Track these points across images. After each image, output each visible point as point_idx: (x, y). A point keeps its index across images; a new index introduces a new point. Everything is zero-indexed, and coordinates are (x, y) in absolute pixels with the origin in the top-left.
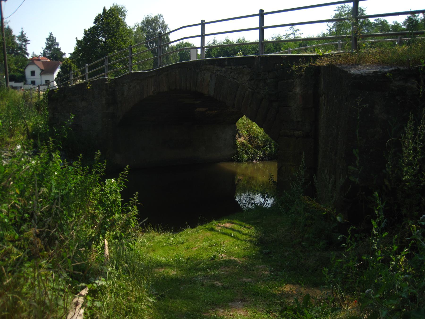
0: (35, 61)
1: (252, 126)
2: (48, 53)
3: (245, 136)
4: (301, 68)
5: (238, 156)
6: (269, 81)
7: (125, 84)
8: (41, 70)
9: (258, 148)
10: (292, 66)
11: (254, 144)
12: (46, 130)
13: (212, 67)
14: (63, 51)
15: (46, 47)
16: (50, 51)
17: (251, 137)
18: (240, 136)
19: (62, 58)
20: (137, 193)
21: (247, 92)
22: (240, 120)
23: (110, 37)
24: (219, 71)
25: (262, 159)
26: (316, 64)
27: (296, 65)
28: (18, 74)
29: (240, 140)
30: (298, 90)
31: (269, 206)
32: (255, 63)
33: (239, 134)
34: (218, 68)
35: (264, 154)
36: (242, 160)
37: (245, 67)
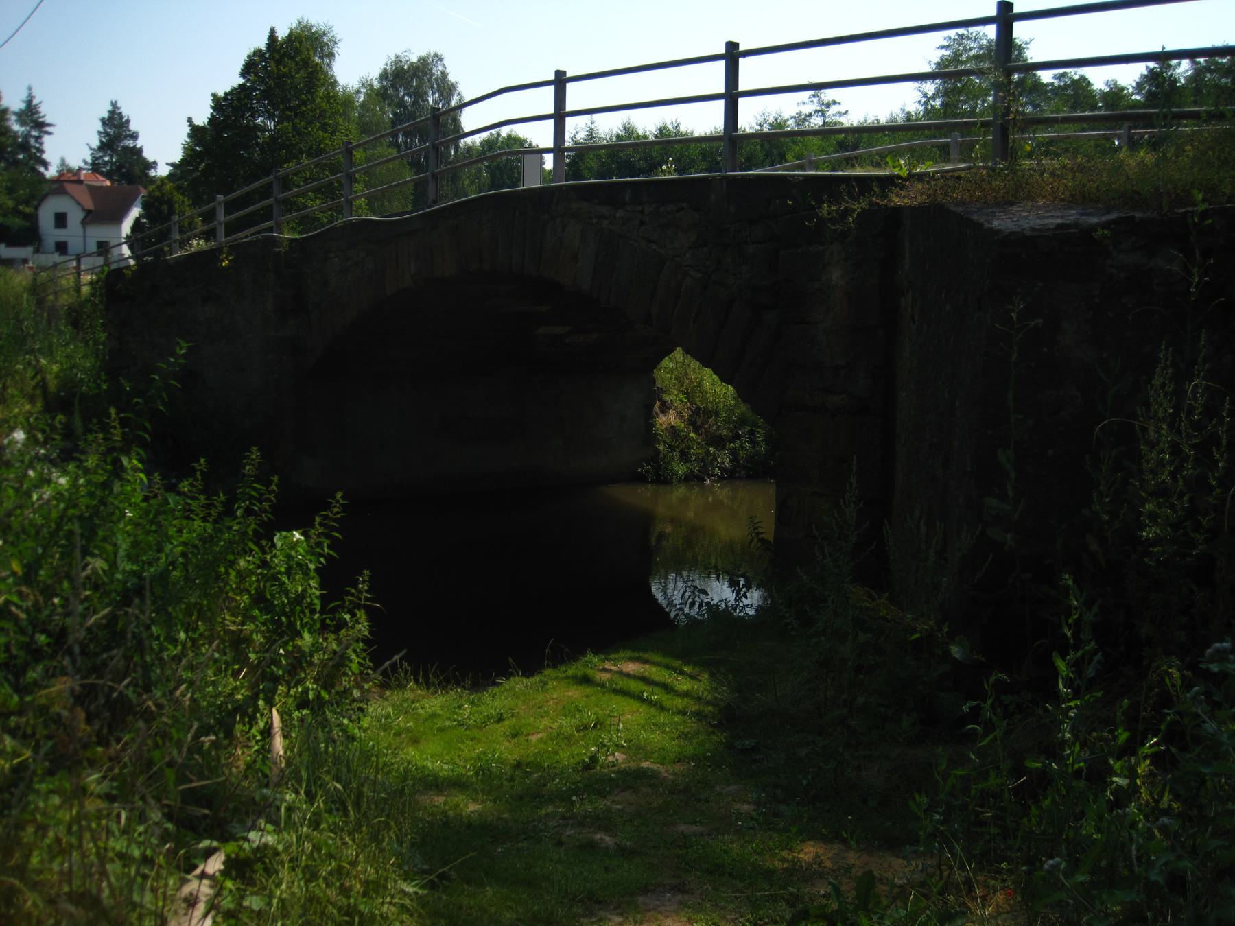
1: (702, 380)
2: (106, 163)
3: (680, 407)
4: (846, 213)
8: (84, 210)
9: (719, 442)
10: (820, 207)
11: (706, 432)
12: (99, 386)
14: (149, 155)
16: (111, 157)
17: (696, 412)
18: (665, 408)
19: (146, 175)
20: (366, 572)
22: (666, 362)
23: (288, 118)
25: (729, 476)
26: (890, 201)
27: (830, 204)
29: (666, 420)
30: (836, 275)
31: (751, 612)
33: (663, 403)
36: (672, 477)
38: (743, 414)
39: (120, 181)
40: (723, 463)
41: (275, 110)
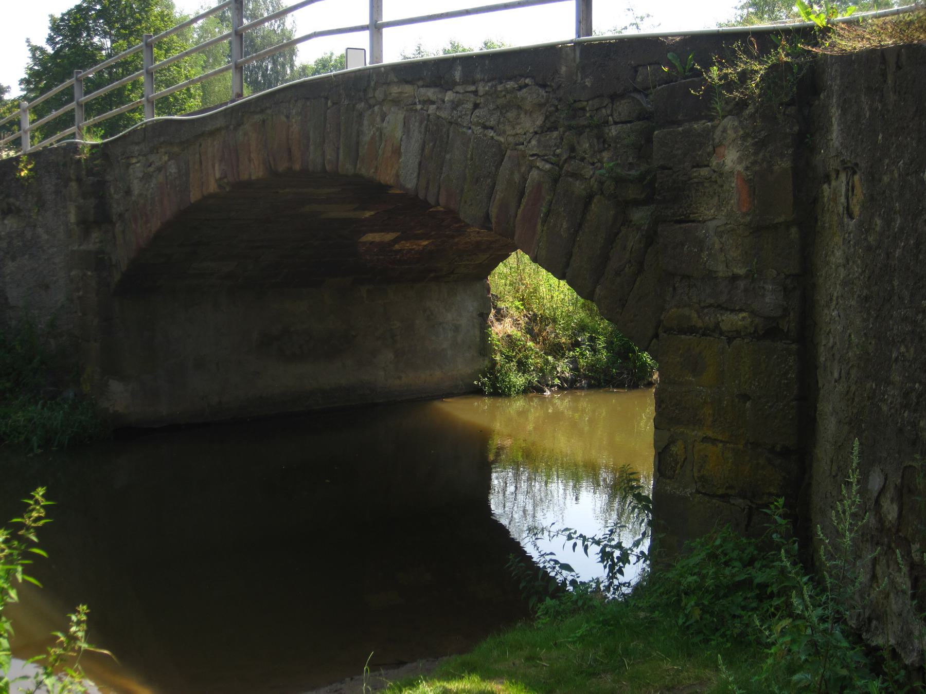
1: (539, 285)
3: (516, 315)
5: (497, 378)
6: (613, 131)
7: (134, 160)
9: (556, 350)
11: (544, 340)
13: (408, 89)
17: (533, 319)
18: (500, 316)
20: (83, 608)
21: (534, 173)
22: (501, 268)
23: (125, 37)
24: (433, 103)
25: (569, 386)
26: (833, 45)
27: (722, 66)
29: (500, 330)
30: (730, 158)
31: (626, 590)
32: (564, 69)
33: (498, 311)
34: (431, 93)
35: (575, 369)
36: (510, 389)
37: (526, 85)
38: (582, 320)
40: (563, 372)
41: (111, 28)
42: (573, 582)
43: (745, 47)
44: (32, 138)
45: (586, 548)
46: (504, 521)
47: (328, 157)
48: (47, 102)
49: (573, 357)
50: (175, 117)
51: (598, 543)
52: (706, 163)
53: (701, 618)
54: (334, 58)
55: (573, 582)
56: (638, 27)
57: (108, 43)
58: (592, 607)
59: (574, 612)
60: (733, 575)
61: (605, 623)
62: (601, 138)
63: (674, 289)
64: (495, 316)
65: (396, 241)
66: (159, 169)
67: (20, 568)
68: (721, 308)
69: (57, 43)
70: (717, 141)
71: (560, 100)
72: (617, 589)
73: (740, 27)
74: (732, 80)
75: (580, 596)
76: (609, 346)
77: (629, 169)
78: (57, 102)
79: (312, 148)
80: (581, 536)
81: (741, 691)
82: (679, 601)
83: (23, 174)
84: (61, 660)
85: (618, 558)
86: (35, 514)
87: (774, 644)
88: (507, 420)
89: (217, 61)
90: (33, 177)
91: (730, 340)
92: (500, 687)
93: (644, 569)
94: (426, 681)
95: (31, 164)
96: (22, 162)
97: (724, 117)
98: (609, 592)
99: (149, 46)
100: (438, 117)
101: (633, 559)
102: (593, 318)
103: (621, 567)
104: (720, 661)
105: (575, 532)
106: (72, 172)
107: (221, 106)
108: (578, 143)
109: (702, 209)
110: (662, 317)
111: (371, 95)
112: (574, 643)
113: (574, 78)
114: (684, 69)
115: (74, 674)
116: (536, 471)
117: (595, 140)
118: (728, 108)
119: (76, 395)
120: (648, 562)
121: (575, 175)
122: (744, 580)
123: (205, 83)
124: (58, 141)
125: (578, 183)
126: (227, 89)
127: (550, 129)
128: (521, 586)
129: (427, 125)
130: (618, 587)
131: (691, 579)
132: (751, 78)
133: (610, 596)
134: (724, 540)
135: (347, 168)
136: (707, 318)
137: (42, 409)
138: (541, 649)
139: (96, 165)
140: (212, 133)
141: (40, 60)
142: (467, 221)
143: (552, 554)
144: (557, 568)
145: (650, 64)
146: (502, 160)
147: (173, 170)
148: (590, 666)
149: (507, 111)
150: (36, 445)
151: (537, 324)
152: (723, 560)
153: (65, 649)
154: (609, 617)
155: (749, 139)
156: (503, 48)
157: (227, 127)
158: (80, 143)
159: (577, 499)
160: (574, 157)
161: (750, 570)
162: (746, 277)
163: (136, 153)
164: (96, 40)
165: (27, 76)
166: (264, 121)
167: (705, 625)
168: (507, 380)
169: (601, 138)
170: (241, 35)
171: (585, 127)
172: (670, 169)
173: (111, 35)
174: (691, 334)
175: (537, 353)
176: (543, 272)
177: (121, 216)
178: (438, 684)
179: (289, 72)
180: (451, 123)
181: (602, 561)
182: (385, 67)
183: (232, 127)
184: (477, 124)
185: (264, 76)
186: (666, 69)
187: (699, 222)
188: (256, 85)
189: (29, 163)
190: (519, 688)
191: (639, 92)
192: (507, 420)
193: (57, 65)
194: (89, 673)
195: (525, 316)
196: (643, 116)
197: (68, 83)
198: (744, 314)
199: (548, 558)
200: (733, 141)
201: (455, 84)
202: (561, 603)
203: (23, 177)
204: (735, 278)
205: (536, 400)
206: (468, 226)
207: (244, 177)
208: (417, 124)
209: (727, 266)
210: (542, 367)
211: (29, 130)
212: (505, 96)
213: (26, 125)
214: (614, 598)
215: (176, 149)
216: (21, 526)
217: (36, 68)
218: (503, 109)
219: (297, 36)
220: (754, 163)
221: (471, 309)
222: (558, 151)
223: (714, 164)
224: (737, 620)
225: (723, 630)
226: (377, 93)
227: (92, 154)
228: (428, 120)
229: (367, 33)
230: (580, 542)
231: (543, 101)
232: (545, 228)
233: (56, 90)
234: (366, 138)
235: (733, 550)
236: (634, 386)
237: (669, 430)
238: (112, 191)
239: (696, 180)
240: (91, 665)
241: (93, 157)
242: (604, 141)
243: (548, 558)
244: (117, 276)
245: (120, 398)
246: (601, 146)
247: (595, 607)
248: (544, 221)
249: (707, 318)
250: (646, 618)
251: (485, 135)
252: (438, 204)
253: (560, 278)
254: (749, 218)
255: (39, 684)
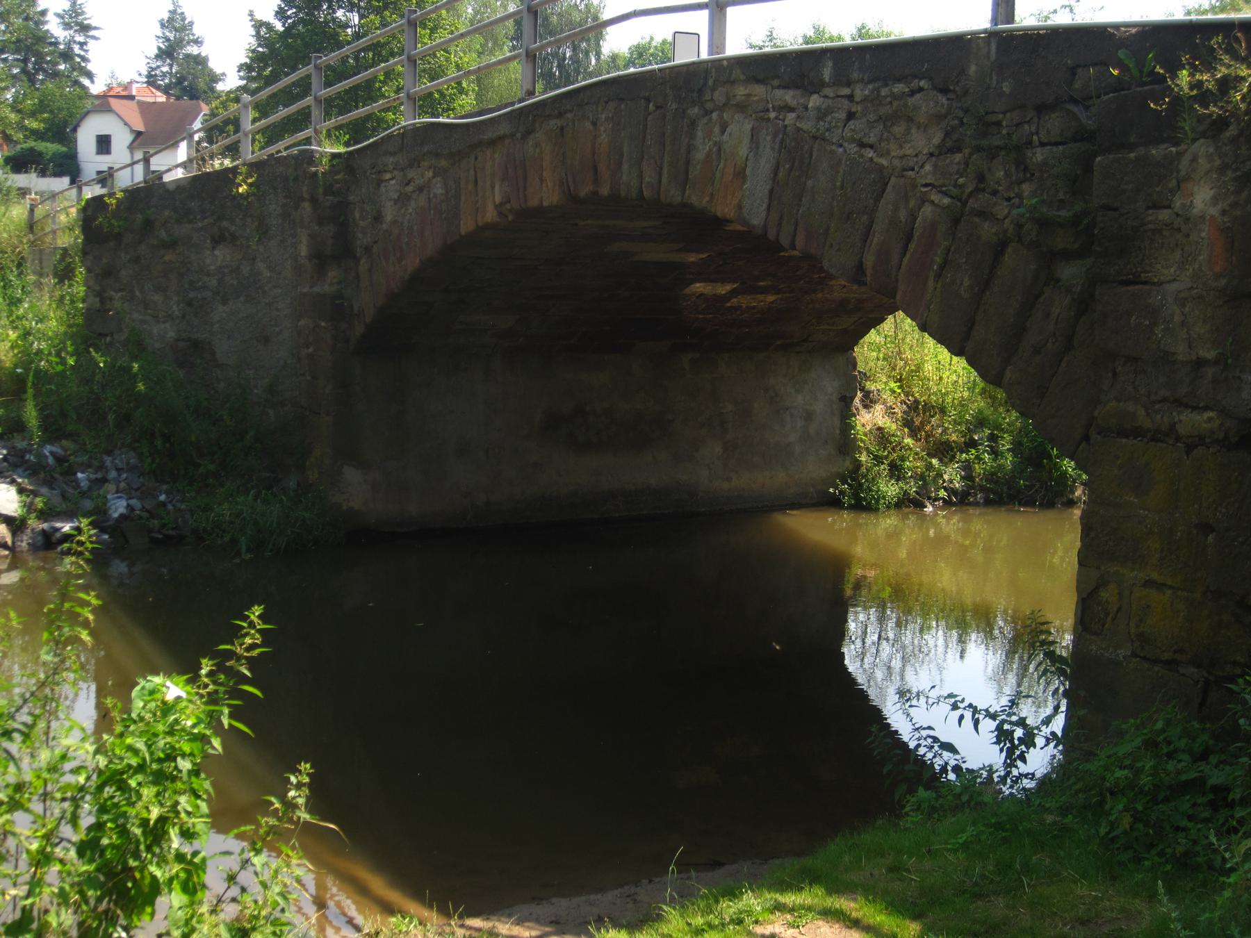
0: (112, 101)
1: (923, 362)
2: (164, 75)
5: (861, 485)
6: (1039, 155)
7: (388, 176)
8: (132, 131)
9: (944, 451)
10: (1174, 77)
11: (928, 436)
12: (63, 362)
13: (759, 90)
14: (215, 65)
15: (156, 51)
16: (171, 66)
17: (914, 407)
19: (212, 90)
20: (305, 767)
21: (927, 210)
22: (872, 336)
24: (792, 110)
25: (959, 500)
27: (1194, 70)
28: (50, 148)
29: (868, 420)
30: (1202, 198)
31: (1028, 784)
32: (973, 68)
33: (867, 394)
34: (789, 97)
35: (968, 477)
36: (877, 501)
37: (921, 89)
39: (178, 98)
40: (951, 481)
42: (957, 769)
43: (1229, 44)
44: (253, 140)
45: (976, 723)
46: (861, 679)
47: (647, 179)
48: (273, 96)
49: (966, 461)
50: (441, 120)
51: (993, 717)
52: (1166, 203)
53: (1131, 828)
54: (654, 44)
55: (957, 769)
56: (1071, 11)
57: (355, 18)
58: (981, 805)
59: (957, 808)
60: (1179, 772)
61: (999, 826)
62: (1021, 164)
63: (1115, 375)
64: (862, 401)
65: (734, 293)
66: (420, 189)
67: (226, 711)
68: (1179, 403)
69: (289, 17)
70: (1183, 173)
71: (967, 111)
72: (1016, 782)
73: (1210, 16)
74: (1208, 90)
75: (965, 789)
76: (1017, 448)
77: (1059, 209)
78: (288, 96)
79: (625, 167)
80: (970, 706)
81: (1187, 933)
82: (1102, 802)
83: (241, 190)
84: (275, 833)
85: (1019, 739)
86: (248, 641)
87: (1232, 870)
88: (872, 543)
89: (498, 45)
90: (254, 194)
91: (1189, 449)
92: (853, 905)
93: (1054, 757)
94: (753, 891)
95: (252, 177)
96: (240, 174)
97: (1194, 140)
98: (1005, 784)
99: (412, 24)
100: (799, 130)
101: (1040, 741)
102: (996, 410)
103: (1023, 752)
104: (1161, 890)
105: (963, 701)
106: (305, 189)
107: (506, 106)
108: (990, 169)
109: (1159, 266)
110: (1096, 414)
111: (708, 97)
112: (955, 851)
113: (987, 80)
114: (1141, 72)
115: (290, 853)
116: (908, 611)
117: (1013, 168)
118: (1201, 128)
119: (299, 484)
120: (1060, 747)
121: (983, 214)
122: (1194, 780)
123: (481, 74)
124: (286, 149)
125: (986, 225)
126: (512, 82)
127: (952, 151)
128: (885, 770)
129: (783, 140)
130: (1018, 778)
131: (1120, 774)
132: (1235, 88)
133: (1006, 790)
134: (1168, 722)
135: (673, 194)
136: (1159, 417)
137: (255, 500)
138: (910, 857)
139: (337, 181)
140: (492, 143)
141: (266, 39)
142: (833, 271)
143: (930, 728)
144: (936, 748)
145: (1094, 65)
146: (883, 191)
147: (438, 189)
148: (976, 884)
149: (893, 124)
150: (244, 548)
151: (918, 415)
152: (1165, 751)
153: (279, 819)
154: (1005, 818)
155: (1229, 173)
156: (893, 38)
157: (513, 135)
158: (317, 151)
159: (962, 657)
160: (984, 190)
161: (1202, 766)
162: (1216, 362)
163: (391, 167)
164: (340, 14)
165: (248, 61)
166: (562, 129)
167: (1137, 839)
168: (875, 488)
169: (1021, 164)
170: (536, 12)
171: (1000, 148)
172: (1116, 209)
173: (359, 8)
174: (1135, 438)
175: (917, 454)
176: (930, 342)
177: (367, 249)
178: (768, 896)
179: (593, 62)
180: (815, 138)
181: (998, 742)
182: (729, 59)
183: (519, 135)
184: (852, 140)
185: (560, 66)
186: (1115, 72)
187: (1154, 284)
188: (550, 82)
189: (249, 175)
190: (878, 907)
191: (1076, 102)
192: (872, 543)
193: (288, 46)
194: (309, 853)
195: (903, 402)
196: (1081, 135)
197: (302, 72)
198: (1211, 414)
199: (924, 733)
200: (1207, 173)
201: (823, 85)
202: (939, 796)
203: (241, 195)
204: (1200, 363)
205: (912, 518)
206: (831, 277)
207: (534, 203)
208: (769, 138)
209: (1190, 347)
210: (922, 473)
211: (250, 131)
212: (891, 103)
213: (247, 125)
214: (1011, 794)
215: (444, 163)
216: (230, 655)
217: (260, 49)
218: (887, 121)
219: (606, 16)
220: (1234, 205)
221: (830, 390)
222: (961, 180)
223: (1178, 204)
224: (1181, 834)
225: (1160, 847)
226: (716, 95)
227: (333, 166)
228: (785, 133)
229: (705, 13)
230: (968, 715)
231: (943, 111)
232: (939, 285)
233: (285, 81)
234: (699, 156)
235: (1180, 738)
236: (1048, 504)
237: (1099, 568)
238: (357, 215)
239: (1151, 226)
240: (311, 841)
241: (333, 170)
242: (1026, 169)
243: (924, 733)
244: (359, 330)
245: (357, 491)
246: (1021, 175)
247: (985, 804)
248: (938, 276)
249: (1159, 417)
250: (1055, 823)
251: (862, 156)
252: (793, 247)
253: (956, 350)
254: (1223, 281)
255: (246, 863)
